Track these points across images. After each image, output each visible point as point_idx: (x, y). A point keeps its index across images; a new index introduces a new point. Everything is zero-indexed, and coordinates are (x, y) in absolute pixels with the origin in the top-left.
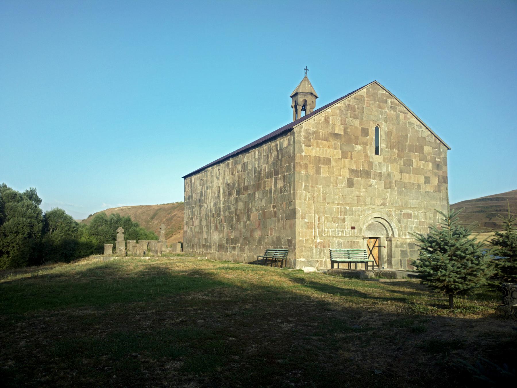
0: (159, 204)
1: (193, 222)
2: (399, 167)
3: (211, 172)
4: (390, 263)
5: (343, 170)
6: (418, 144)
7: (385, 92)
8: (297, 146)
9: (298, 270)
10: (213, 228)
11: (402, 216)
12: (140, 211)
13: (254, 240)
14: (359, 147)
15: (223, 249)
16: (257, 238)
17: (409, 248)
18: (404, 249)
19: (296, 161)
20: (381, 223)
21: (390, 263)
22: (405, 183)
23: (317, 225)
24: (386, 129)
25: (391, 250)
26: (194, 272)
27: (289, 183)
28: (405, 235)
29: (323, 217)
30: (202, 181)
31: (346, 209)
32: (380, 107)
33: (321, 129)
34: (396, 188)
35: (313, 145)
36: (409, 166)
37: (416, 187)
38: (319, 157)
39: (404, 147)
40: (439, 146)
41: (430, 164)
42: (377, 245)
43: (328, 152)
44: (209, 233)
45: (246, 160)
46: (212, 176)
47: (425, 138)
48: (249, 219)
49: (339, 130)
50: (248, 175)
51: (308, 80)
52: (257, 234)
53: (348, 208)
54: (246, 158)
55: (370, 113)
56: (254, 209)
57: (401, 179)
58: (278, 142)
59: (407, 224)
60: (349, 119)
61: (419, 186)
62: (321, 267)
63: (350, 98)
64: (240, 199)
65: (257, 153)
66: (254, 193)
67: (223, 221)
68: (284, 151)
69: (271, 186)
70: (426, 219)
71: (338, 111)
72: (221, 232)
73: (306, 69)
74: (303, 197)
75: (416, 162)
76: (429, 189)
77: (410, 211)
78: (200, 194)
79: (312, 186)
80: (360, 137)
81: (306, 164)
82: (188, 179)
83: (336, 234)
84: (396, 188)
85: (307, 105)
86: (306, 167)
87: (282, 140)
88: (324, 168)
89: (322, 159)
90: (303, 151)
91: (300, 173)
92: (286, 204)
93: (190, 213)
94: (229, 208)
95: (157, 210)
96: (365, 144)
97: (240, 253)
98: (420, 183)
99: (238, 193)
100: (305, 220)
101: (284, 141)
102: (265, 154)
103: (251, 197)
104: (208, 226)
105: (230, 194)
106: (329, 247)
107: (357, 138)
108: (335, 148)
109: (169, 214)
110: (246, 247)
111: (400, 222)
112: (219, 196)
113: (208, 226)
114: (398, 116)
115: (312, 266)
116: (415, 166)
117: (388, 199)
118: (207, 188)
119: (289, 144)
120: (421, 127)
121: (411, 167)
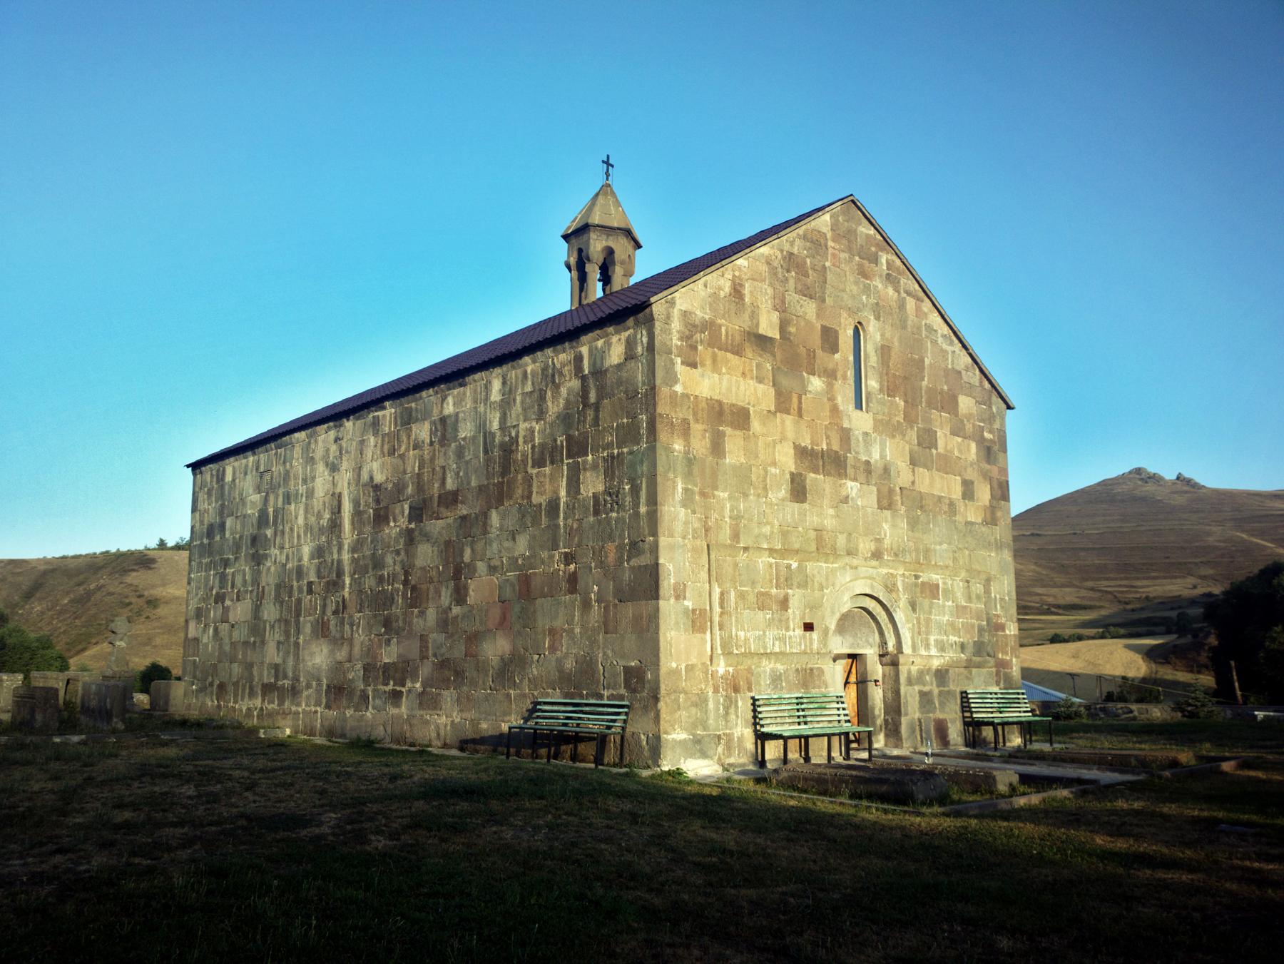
0: (49, 556)
1: (226, 610)
2: (907, 447)
3: (307, 448)
4: (893, 731)
5: (776, 446)
6: (946, 387)
7: (872, 231)
8: (660, 362)
9: (669, 773)
10: (308, 629)
11: (918, 590)
13: (481, 667)
14: (816, 383)
15: (350, 699)
16: (495, 662)
17: (938, 686)
18: (926, 689)
19: (660, 410)
20: (871, 614)
21: (893, 731)
22: (921, 496)
23: (716, 619)
24: (878, 338)
25: (897, 693)
27: (632, 481)
28: (927, 646)
29: (733, 594)
30: (267, 477)
31: (789, 567)
32: (864, 274)
33: (723, 317)
34: (903, 509)
35: (703, 365)
37: (945, 508)
38: (720, 403)
39: (915, 393)
40: (990, 399)
41: (973, 445)
42: (853, 679)
43: (742, 388)
44: (291, 646)
45: (449, 408)
48: (460, 596)
49: (768, 325)
50: (460, 453)
51: (613, 194)
52: (496, 648)
53: (795, 565)
54: (451, 403)
55: (841, 286)
56: (481, 566)
57: (913, 483)
59: (930, 613)
60: (792, 297)
61: (951, 504)
62: (729, 756)
63: (794, 234)
64: (427, 537)
65: (496, 385)
66: (485, 515)
68: (611, 378)
69: (556, 492)
70: (969, 599)
71: (764, 268)
73: (607, 163)
74: (678, 527)
75: (945, 441)
76: (972, 513)
77: (936, 577)
78: (255, 521)
79: (703, 494)
80: (819, 353)
81: (685, 422)
82: (209, 472)
83: (765, 648)
84: (903, 509)
85: (613, 263)
87: (600, 343)
88: (733, 441)
89: (726, 407)
90: (676, 381)
91: (669, 450)
92: (620, 548)
93: (214, 581)
94: (378, 563)
95: (45, 573)
96: (830, 375)
97: (419, 713)
98: (954, 497)
99: (417, 513)
100: (686, 603)
101: (614, 347)
102: (529, 388)
103: (472, 527)
104: (287, 622)
105: (381, 518)
106: (750, 690)
107: (811, 354)
108: (760, 380)
109: (79, 585)
110: (445, 693)
111: (914, 610)
112: (335, 525)
113: (290, 622)
114: (902, 306)
115: (704, 755)
116: (941, 450)
117: (887, 542)
118: (288, 499)
119: (630, 356)
120: (951, 343)
121: (934, 451)
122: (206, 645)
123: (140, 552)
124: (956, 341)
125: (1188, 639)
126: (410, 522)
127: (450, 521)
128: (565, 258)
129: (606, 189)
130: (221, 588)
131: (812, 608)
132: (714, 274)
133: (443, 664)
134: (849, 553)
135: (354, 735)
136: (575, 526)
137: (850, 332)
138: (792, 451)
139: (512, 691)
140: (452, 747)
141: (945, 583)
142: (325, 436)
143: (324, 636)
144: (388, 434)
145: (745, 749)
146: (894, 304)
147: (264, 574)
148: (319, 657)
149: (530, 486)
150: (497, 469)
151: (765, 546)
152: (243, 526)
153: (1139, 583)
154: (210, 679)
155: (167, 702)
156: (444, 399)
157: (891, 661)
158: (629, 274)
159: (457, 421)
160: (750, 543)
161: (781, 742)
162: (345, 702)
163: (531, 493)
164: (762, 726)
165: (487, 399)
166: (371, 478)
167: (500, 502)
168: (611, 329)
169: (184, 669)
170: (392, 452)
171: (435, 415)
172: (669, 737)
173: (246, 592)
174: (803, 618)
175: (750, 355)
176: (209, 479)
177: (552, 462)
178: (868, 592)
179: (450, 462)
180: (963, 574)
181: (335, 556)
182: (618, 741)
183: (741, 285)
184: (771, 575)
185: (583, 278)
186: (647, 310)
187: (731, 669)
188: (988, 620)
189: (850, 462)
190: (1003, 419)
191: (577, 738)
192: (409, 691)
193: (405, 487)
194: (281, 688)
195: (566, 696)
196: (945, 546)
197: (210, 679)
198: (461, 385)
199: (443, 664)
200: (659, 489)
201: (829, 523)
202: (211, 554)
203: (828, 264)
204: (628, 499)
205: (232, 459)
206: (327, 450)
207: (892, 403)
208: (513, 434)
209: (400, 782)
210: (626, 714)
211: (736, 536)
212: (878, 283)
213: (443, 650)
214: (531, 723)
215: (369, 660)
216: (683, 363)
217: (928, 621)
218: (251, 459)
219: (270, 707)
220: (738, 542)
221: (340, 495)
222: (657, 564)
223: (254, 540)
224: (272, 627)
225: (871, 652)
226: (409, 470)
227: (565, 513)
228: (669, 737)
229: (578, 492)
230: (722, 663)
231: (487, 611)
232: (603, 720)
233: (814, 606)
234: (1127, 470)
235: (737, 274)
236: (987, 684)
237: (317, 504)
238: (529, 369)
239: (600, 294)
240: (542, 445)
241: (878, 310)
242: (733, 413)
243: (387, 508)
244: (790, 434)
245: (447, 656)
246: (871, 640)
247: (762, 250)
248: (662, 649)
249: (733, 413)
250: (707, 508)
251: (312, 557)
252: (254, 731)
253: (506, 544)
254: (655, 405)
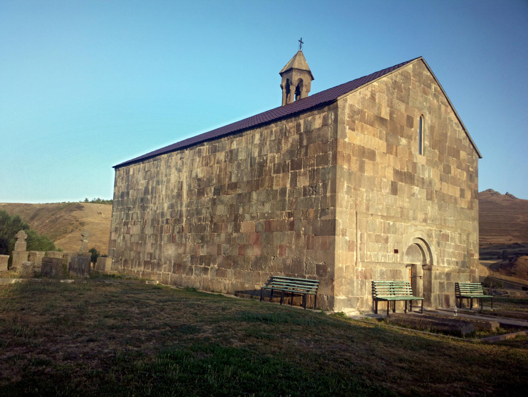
0: (41, 203)
1: (129, 229)
2: (439, 173)
5: (385, 168)
6: (455, 147)
7: (429, 74)
8: (340, 127)
10: (166, 239)
11: (441, 237)
12: (17, 209)
13: (246, 260)
14: (404, 141)
15: (184, 270)
16: (253, 258)
17: (447, 280)
18: (442, 281)
20: (421, 247)
21: (427, 299)
23: (359, 246)
24: (430, 122)
25: (430, 282)
27: (324, 181)
28: (443, 263)
29: (366, 234)
30: (149, 173)
32: (425, 93)
33: (367, 108)
34: (436, 200)
35: (357, 130)
36: (448, 173)
37: (453, 201)
38: (363, 148)
40: (472, 152)
41: (465, 173)
43: (373, 142)
45: (234, 146)
46: (169, 167)
47: (461, 140)
48: (237, 229)
49: (385, 113)
50: (239, 166)
51: (303, 54)
52: (253, 252)
53: (391, 223)
56: (247, 216)
57: (441, 189)
58: (302, 121)
59: (445, 248)
60: (396, 101)
61: (456, 199)
62: (362, 307)
63: (397, 73)
64: (222, 202)
65: (257, 136)
66: (250, 194)
67: (186, 230)
68: (314, 135)
69: (285, 185)
70: (461, 242)
71: (384, 87)
72: (179, 245)
73: (301, 41)
74: (344, 203)
75: (454, 171)
76: (463, 204)
77: (448, 232)
78: (143, 192)
79: (355, 189)
80: (405, 127)
81: (349, 155)
82: (122, 170)
83: (378, 260)
85: (302, 86)
86: (349, 161)
87: (310, 118)
88: (368, 165)
89: (366, 150)
90: (346, 137)
92: (316, 211)
94: (199, 212)
95: (39, 210)
96: (409, 138)
97: (215, 278)
98: (457, 196)
99: (217, 192)
100: (346, 238)
101: (317, 120)
102: (273, 138)
103: (244, 199)
104: (156, 235)
105: (201, 193)
106: (371, 278)
107: (402, 128)
108: (381, 138)
109: (53, 215)
110: (229, 270)
111: (439, 246)
112: (179, 195)
113: (158, 234)
114: (440, 108)
115: (352, 306)
116: (452, 175)
117: (429, 215)
118: (158, 183)
119: (325, 124)
120: (458, 127)
121: (450, 175)
122: (119, 243)
123: (78, 203)
124: (460, 126)
125: (507, 262)
126: (214, 195)
127: (233, 195)
128: (281, 83)
129: (299, 53)
130: (127, 219)
131: (398, 243)
132: (364, 89)
133: (228, 257)
134: (414, 219)
135: (186, 285)
136: (294, 200)
137: (419, 119)
138: (392, 172)
139: (260, 272)
140: (231, 294)
141: (451, 235)
142: (176, 157)
143: (173, 242)
144: (205, 157)
145: (369, 305)
146: (436, 107)
147: (146, 215)
148: (170, 251)
149: (272, 182)
150: (256, 173)
151: (380, 214)
152: (137, 193)
153: (487, 237)
154: (121, 257)
155: (104, 267)
156: (232, 142)
157: (428, 268)
158: (308, 91)
159: (238, 152)
160: (373, 212)
161: (387, 302)
162: (182, 271)
163: (272, 185)
164: (377, 295)
165: (252, 142)
166: (197, 176)
167: (257, 188)
168: (316, 112)
169: (109, 253)
170: (207, 165)
171: (228, 149)
172: (338, 297)
173: (138, 222)
174: (394, 247)
175: (377, 127)
176: (122, 173)
177: (284, 172)
178: (420, 237)
179: (234, 170)
180: (459, 231)
181: (179, 209)
182: (313, 297)
183: (375, 94)
184: (381, 227)
185: (288, 91)
186: (335, 104)
187: (364, 269)
188: (468, 252)
189: (416, 178)
190: (477, 162)
191: (293, 295)
192: (212, 268)
193: (212, 180)
194: (153, 263)
195: (287, 275)
196: (452, 218)
197: (121, 257)
198: (240, 136)
199: (228, 257)
200: (337, 185)
201: (406, 205)
202: (122, 205)
203: (410, 87)
204: (321, 189)
205: (133, 165)
206: (177, 163)
207: (434, 152)
208: (265, 158)
209: (227, 311)
210: (318, 286)
211: (368, 209)
212: (430, 97)
213: (228, 251)
214: (270, 286)
215: (193, 254)
216: (349, 128)
217: (444, 251)
218: (142, 165)
219: (148, 271)
220: (368, 211)
221: (182, 182)
222: (335, 220)
223: (142, 200)
224: (150, 237)
225: (419, 264)
226: (214, 173)
227: (289, 194)
228: (338, 297)
229: (296, 185)
230: (360, 266)
231: (249, 236)
232: (305, 288)
233: (399, 242)
234: (485, 190)
235: (373, 89)
236: (466, 280)
237: (171, 186)
238: (274, 130)
239: (295, 100)
240: (279, 164)
241: (430, 109)
242: (369, 153)
243: (203, 189)
244: (392, 164)
245: (230, 254)
246: (419, 258)
247: (384, 79)
248: (336, 258)
249: (369, 153)
250: (357, 195)
251: (168, 208)
252: (143, 281)
253: (259, 207)
254: (337, 147)
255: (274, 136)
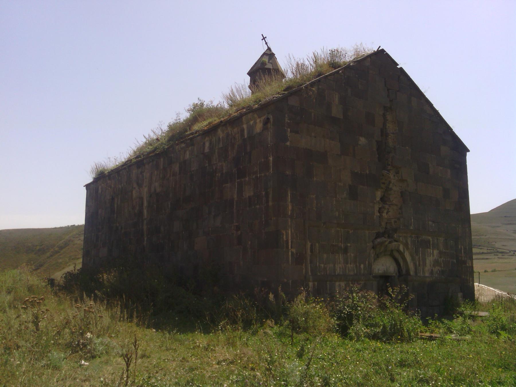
0: (76, 225)
26: (142, 161)
49: (336, 111)
102: (221, 145)
216: (291, 132)
255: (221, 143)
